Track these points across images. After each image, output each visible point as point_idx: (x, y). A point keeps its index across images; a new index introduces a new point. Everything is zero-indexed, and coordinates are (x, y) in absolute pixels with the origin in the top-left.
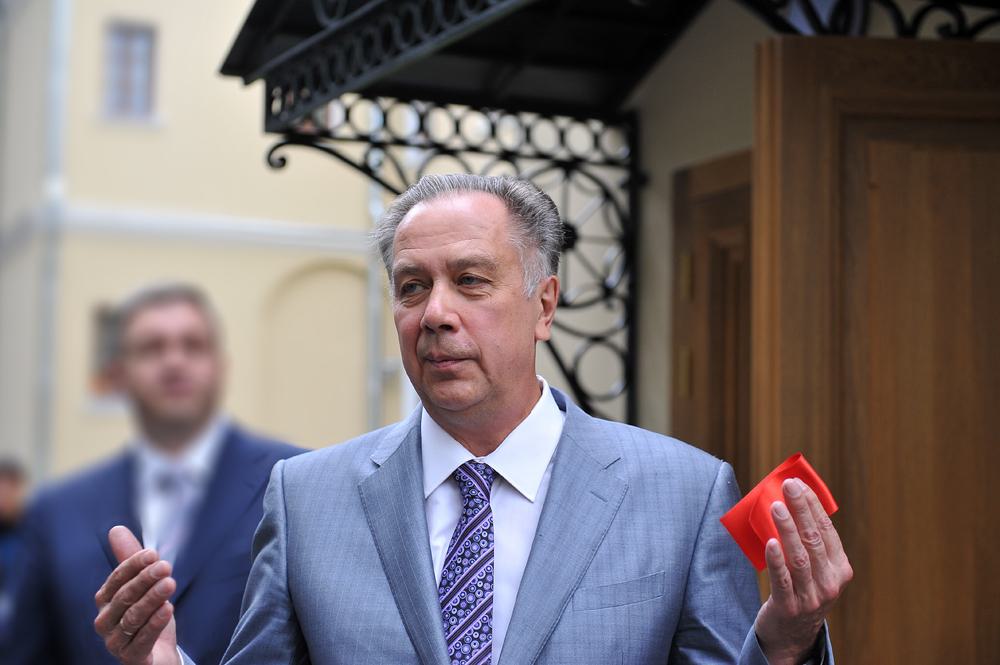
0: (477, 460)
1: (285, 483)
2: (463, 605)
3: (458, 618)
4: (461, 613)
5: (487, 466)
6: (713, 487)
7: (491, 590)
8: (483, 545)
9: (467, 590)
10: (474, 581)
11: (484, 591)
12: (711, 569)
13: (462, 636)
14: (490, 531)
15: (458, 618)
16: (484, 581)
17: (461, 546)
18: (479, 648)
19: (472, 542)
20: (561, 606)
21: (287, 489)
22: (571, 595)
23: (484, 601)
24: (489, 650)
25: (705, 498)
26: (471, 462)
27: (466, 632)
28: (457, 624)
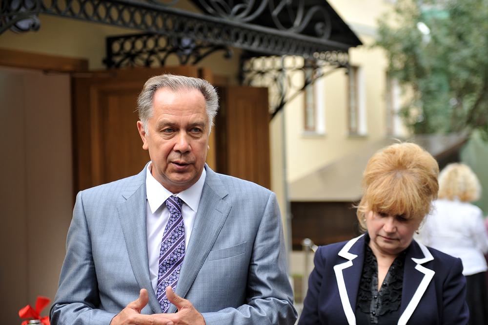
0: (174, 195)
1: (84, 204)
2: (173, 237)
3: (171, 243)
4: (172, 241)
5: (179, 199)
6: (266, 205)
7: (184, 253)
8: (178, 256)
9: (173, 253)
10: (176, 249)
11: (181, 253)
12: (266, 216)
13: (174, 229)
14: (182, 227)
15: (171, 243)
16: (181, 249)
17: (170, 234)
18: (181, 256)
19: (175, 232)
20: (203, 260)
21: (85, 207)
22: (207, 255)
23: (181, 258)
24: (184, 237)
25: (263, 209)
26: (172, 196)
27: (175, 249)
28: (170, 267)
